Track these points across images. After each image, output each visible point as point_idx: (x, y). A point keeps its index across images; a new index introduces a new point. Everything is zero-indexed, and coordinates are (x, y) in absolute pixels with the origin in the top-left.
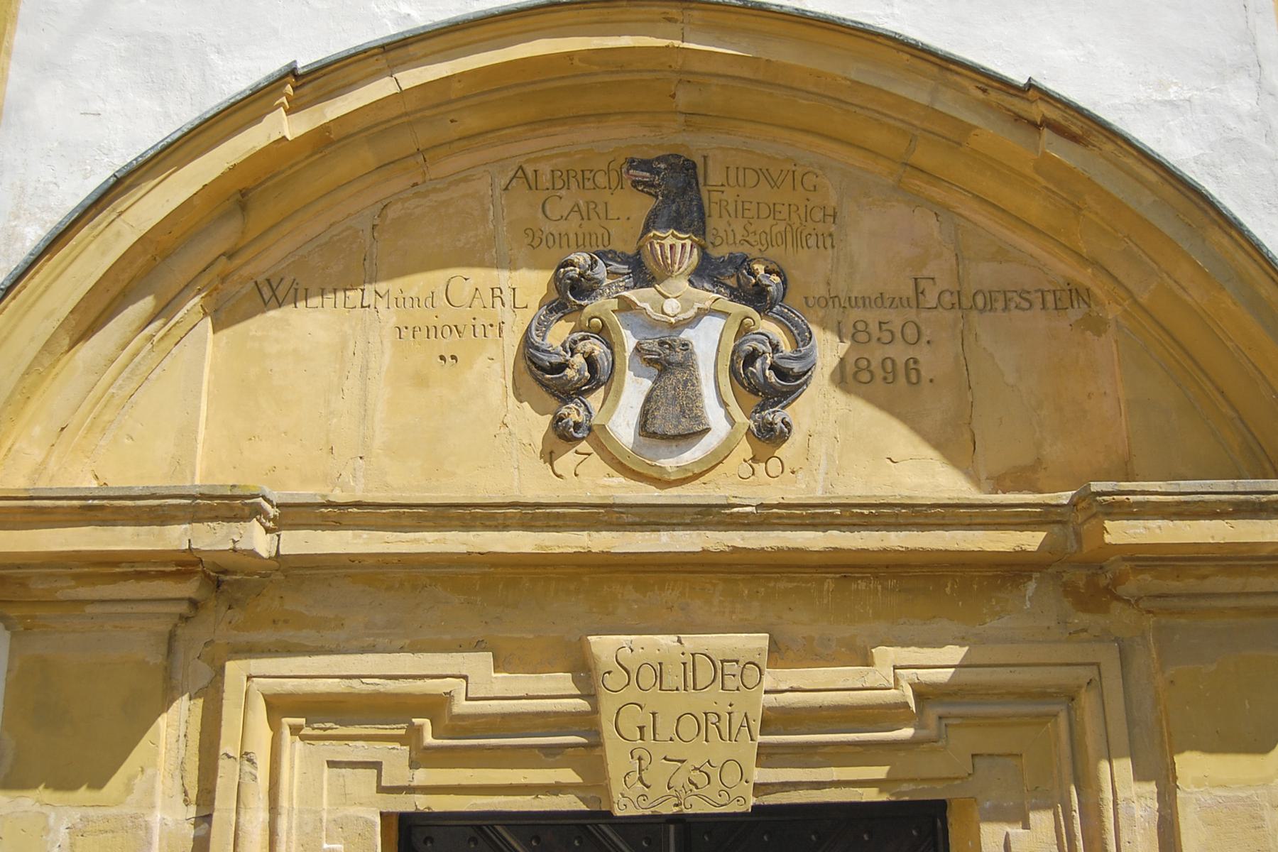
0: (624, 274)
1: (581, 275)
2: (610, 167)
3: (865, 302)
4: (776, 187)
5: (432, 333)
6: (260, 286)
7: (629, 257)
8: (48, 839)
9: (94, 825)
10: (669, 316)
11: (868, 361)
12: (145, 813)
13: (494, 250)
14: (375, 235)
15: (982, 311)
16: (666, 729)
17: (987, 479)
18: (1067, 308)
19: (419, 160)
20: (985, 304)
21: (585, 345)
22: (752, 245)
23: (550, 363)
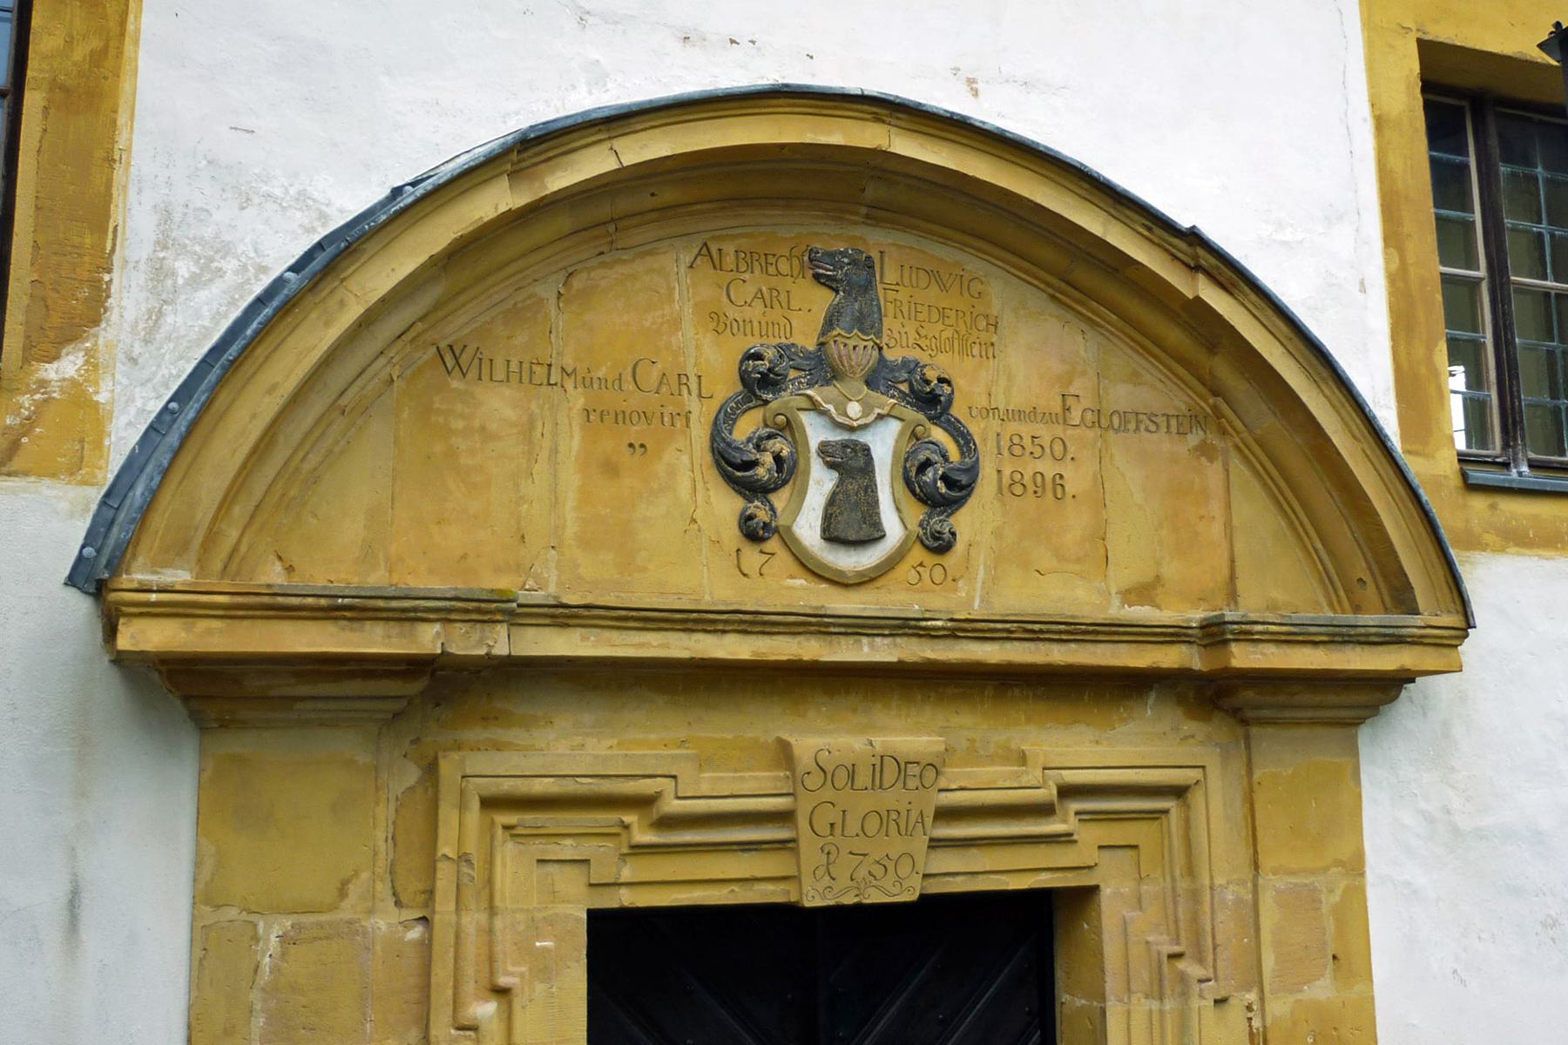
0: (804, 370)
1: (770, 370)
2: (793, 254)
3: (1019, 415)
4: (945, 291)
5: (620, 417)
6: (442, 353)
7: (810, 353)
8: (259, 948)
9: (307, 932)
10: (851, 418)
11: (1022, 474)
12: (361, 917)
13: (680, 334)
14: (561, 305)
15: (1117, 431)
16: (853, 826)
17: (1116, 593)
18: (1186, 434)
19: (610, 230)
20: (1120, 424)
21: (775, 444)
22: (923, 350)
23: (742, 460)
